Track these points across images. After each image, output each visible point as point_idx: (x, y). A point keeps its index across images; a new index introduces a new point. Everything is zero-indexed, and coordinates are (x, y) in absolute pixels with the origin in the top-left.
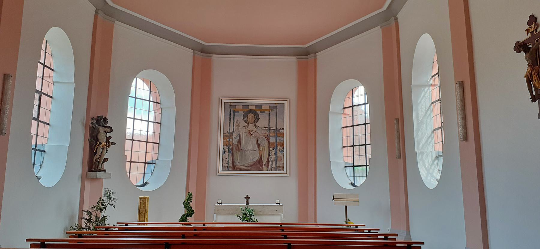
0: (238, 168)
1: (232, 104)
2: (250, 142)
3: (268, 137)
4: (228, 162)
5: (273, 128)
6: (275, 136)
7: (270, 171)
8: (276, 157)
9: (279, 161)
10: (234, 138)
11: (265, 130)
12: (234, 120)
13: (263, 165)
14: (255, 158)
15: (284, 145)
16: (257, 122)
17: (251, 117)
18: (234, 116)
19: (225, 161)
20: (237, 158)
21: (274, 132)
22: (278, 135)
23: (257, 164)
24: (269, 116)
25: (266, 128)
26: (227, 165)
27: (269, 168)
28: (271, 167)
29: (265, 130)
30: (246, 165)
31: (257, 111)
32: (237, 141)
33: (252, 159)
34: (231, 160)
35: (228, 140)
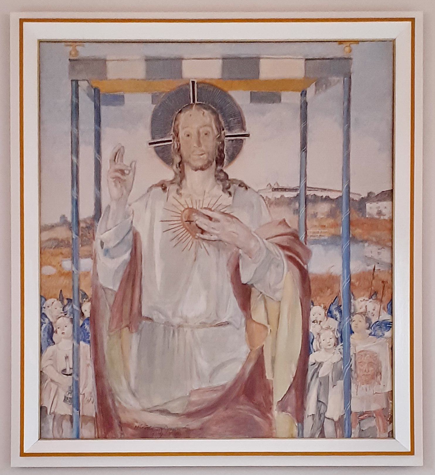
0: (129, 425)
1: (84, 52)
2: (196, 277)
3: (301, 244)
4: (71, 392)
5: (324, 194)
6: (340, 236)
7: (312, 437)
8: (346, 358)
9: (367, 382)
10: (100, 252)
11: (278, 203)
12: (98, 150)
13: (269, 405)
14: (223, 365)
15: (392, 288)
16: (232, 158)
17: (196, 126)
18: (98, 121)
19: (54, 386)
20: (125, 367)
21: (332, 214)
22: (357, 231)
23: (236, 400)
24: (304, 118)
25: (287, 195)
26: (65, 409)
27: (308, 422)
28: (320, 415)
29: (278, 203)
30: (176, 407)
31: (233, 93)
32: (121, 273)
33: (207, 373)
34: (91, 381)
35: (67, 264)
